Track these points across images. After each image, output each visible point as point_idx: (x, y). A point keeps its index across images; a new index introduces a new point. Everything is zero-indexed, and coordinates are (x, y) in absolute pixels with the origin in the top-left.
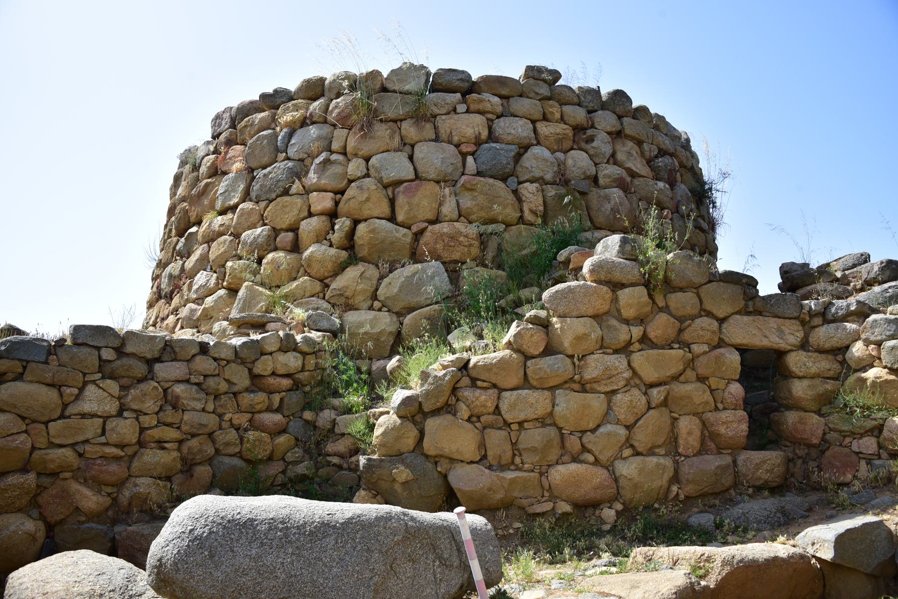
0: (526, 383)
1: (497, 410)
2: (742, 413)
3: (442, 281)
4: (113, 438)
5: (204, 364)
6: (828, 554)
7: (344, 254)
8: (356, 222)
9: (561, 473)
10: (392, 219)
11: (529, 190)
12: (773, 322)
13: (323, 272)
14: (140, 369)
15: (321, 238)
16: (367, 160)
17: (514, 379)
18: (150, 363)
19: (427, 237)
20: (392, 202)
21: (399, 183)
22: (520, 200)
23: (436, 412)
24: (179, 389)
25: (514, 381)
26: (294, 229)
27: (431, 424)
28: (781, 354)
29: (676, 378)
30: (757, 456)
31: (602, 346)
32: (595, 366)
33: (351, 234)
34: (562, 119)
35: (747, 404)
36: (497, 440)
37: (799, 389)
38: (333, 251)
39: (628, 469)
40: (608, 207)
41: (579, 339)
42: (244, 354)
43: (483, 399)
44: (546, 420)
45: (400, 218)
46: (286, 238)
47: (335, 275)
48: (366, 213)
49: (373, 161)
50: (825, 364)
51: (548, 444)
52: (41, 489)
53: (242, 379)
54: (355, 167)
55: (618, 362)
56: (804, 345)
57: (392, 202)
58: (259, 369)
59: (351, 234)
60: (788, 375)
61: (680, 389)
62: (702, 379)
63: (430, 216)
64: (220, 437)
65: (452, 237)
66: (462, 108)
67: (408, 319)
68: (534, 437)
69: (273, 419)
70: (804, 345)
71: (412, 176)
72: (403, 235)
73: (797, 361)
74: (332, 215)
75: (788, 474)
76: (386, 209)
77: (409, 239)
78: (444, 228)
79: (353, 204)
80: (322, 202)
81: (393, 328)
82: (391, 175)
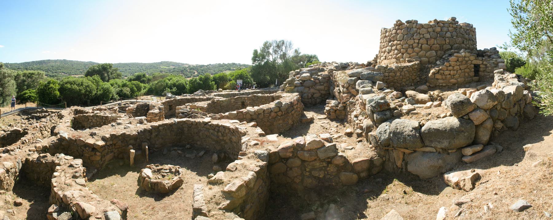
0: (447, 70)
1: (444, 73)
2: (474, 73)
3: (435, 54)
4: (400, 78)
5: (408, 69)
6: (327, 74)
7: (420, 49)
8: (422, 44)
9: (452, 80)
10: (427, 44)
11: (447, 39)
12: (479, 61)
13: (417, 52)
14: (402, 70)
15: (417, 47)
16: (423, 35)
17: (446, 69)
18: (403, 69)
19: (433, 47)
20: (427, 41)
21: (428, 38)
22: (446, 41)
23: (436, 73)
24: (406, 72)
25: (446, 70)
26: (412, 45)
27: (436, 75)
28: (479, 65)
29: (465, 69)
30: (475, 78)
31: (456, 65)
32: (455, 68)
33: (421, 46)
34: (452, 27)
35: (475, 71)
36: (444, 77)
37: (481, 69)
38: (419, 49)
39: (459, 80)
40: (458, 41)
41: (454, 64)
42: (412, 66)
43: (442, 72)
44: (450, 74)
45: (429, 44)
46: (411, 46)
47: (419, 52)
48: (424, 43)
49: (424, 35)
50: (484, 66)
51: (450, 78)
52: (394, 84)
53: (412, 70)
54: (421, 36)
55: (458, 67)
56: (482, 64)
57: (427, 41)
58: (413, 68)
59: (421, 46)
60: (480, 67)
61: (466, 70)
62: (469, 69)
63: (433, 44)
64: (410, 77)
65: (436, 47)
66: (437, 26)
67: (430, 59)
68: (448, 76)
69: (415, 74)
70: (482, 64)
71: (430, 37)
72: (429, 47)
73: (481, 66)
74: (418, 43)
75: (479, 80)
76: (426, 43)
77: (430, 47)
78: (435, 46)
79: (421, 42)
80: (417, 41)
81: (428, 60)
82: (427, 37)
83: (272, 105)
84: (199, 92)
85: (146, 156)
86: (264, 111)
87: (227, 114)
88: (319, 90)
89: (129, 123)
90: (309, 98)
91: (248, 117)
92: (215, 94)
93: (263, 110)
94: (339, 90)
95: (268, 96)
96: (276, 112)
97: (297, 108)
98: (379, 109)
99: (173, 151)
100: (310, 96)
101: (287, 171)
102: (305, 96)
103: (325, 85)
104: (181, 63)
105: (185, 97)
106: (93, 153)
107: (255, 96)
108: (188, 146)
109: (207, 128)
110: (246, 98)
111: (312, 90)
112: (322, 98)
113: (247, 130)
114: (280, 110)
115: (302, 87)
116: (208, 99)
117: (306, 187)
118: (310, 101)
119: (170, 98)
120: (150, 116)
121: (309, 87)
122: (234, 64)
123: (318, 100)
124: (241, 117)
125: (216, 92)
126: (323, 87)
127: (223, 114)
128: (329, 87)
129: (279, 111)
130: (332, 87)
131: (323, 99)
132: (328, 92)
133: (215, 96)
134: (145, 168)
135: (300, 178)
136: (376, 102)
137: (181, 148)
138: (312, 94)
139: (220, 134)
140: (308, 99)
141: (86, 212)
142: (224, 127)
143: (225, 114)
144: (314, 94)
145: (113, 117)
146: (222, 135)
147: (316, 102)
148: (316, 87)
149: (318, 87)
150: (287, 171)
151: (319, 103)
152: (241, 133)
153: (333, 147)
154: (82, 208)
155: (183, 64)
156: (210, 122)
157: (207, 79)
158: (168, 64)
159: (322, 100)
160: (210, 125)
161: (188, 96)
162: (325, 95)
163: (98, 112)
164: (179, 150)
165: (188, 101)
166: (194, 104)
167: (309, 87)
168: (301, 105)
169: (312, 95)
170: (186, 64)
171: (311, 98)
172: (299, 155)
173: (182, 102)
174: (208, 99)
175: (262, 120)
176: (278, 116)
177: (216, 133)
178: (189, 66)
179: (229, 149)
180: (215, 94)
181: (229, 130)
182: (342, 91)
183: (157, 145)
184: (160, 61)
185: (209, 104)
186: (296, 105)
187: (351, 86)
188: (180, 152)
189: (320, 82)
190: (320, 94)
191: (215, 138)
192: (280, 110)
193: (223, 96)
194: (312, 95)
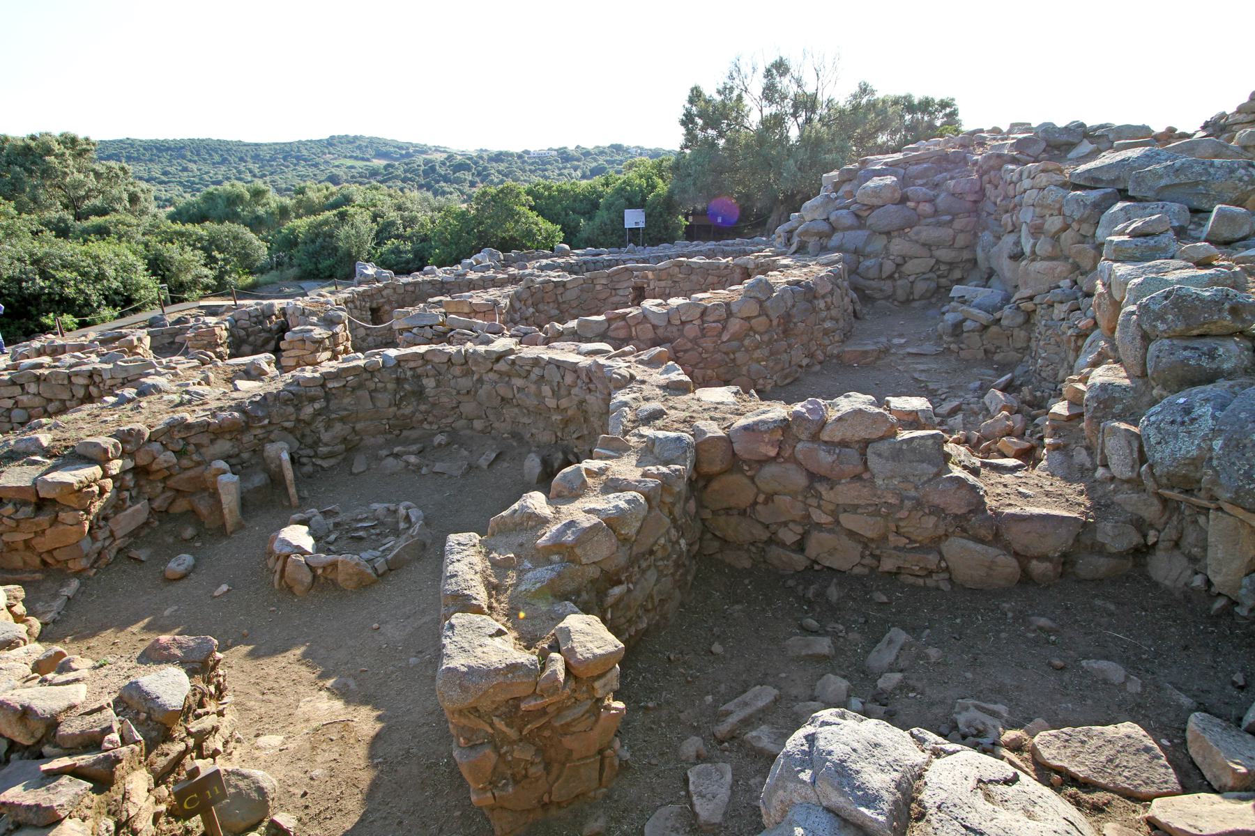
83: (733, 293)
84: (483, 257)
85: (286, 489)
86: (704, 312)
87: (573, 324)
88: (927, 246)
89: (199, 384)
90: (884, 276)
91: (647, 332)
92: (544, 262)
93: (699, 310)
94: (1017, 243)
95: (727, 266)
96: (748, 319)
97: (828, 309)
98: (1180, 327)
99: (391, 459)
100: (889, 267)
101: (755, 503)
102: (868, 268)
103: (959, 224)
104: (416, 146)
105: (428, 278)
106: (44, 519)
107: (680, 265)
108: (440, 439)
109: (500, 373)
110: (650, 274)
111: (898, 246)
112: (939, 277)
113: (631, 371)
114: (763, 312)
115: (859, 232)
116: (514, 280)
117: (815, 562)
118: (887, 286)
119: (367, 283)
120: (293, 353)
121: (888, 233)
122: (617, 148)
123: (921, 287)
124: (622, 334)
125: (546, 257)
126: (951, 231)
127: (559, 326)
128: (975, 235)
129: (759, 315)
130: (987, 233)
131: (943, 281)
132: (966, 255)
133: (542, 268)
134: (286, 525)
135: (799, 529)
136: (1170, 293)
137: (414, 448)
138: (899, 260)
139: (546, 390)
140: (880, 279)
141: (40, 711)
142: (559, 365)
143: (565, 326)
144: (905, 259)
145: (125, 369)
146: (553, 391)
147: (912, 293)
148: (917, 233)
149: (927, 233)
150: (755, 503)
151: (922, 297)
152: (611, 379)
153: (930, 442)
154: (15, 709)
155: (423, 150)
156: (511, 351)
157: (500, 204)
158: (359, 147)
159: (939, 287)
160: (513, 362)
161: (441, 274)
162: (952, 265)
163: (46, 360)
164: (410, 453)
165: (442, 287)
166: (461, 297)
167: (888, 233)
168: (847, 300)
169: (898, 265)
170: (437, 150)
171: (891, 277)
172: (800, 457)
173: (415, 295)
174: (514, 280)
175: (696, 344)
176: (756, 332)
177: (533, 388)
178: (450, 157)
179: (578, 438)
180: (544, 262)
181: (575, 375)
182: (1027, 250)
183: (326, 445)
184: (325, 136)
185: (516, 297)
186: (823, 297)
187: (1075, 226)
188: (412, 459)
189: (936, 211)
190: (933, 261)
191: (531, 402)
192: (763, 312)
193: (570, 269)
194: (898, 265)
